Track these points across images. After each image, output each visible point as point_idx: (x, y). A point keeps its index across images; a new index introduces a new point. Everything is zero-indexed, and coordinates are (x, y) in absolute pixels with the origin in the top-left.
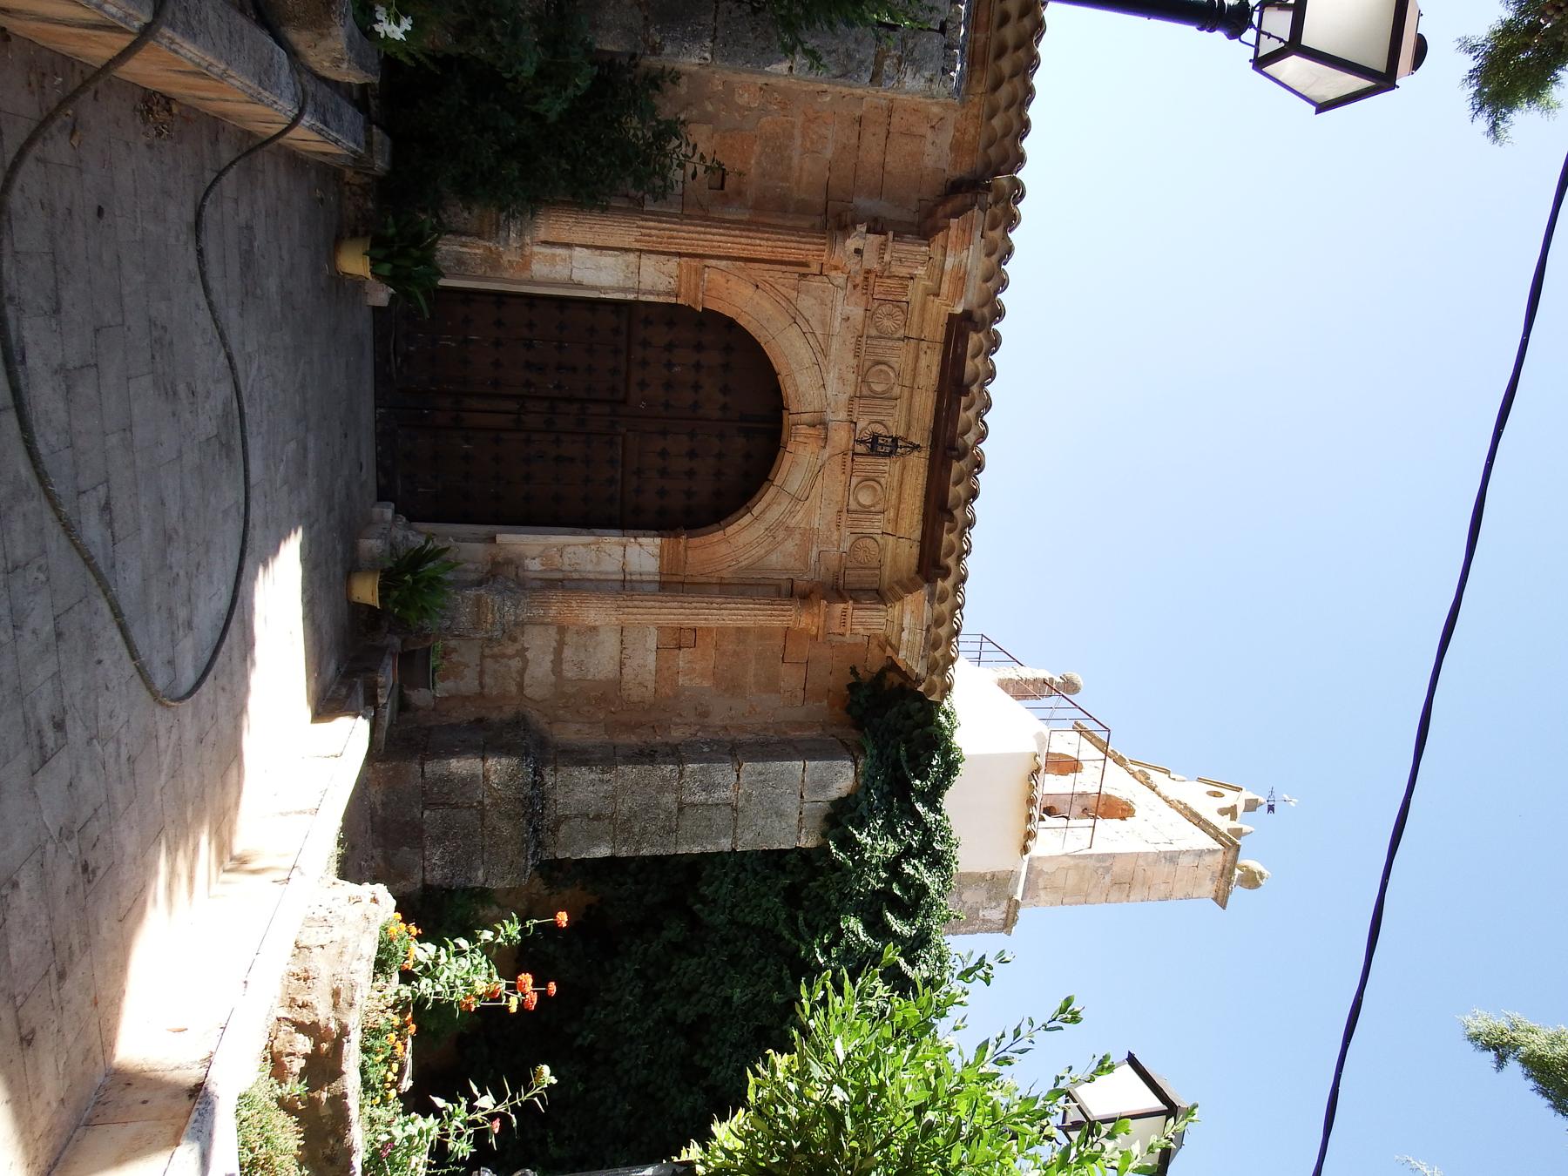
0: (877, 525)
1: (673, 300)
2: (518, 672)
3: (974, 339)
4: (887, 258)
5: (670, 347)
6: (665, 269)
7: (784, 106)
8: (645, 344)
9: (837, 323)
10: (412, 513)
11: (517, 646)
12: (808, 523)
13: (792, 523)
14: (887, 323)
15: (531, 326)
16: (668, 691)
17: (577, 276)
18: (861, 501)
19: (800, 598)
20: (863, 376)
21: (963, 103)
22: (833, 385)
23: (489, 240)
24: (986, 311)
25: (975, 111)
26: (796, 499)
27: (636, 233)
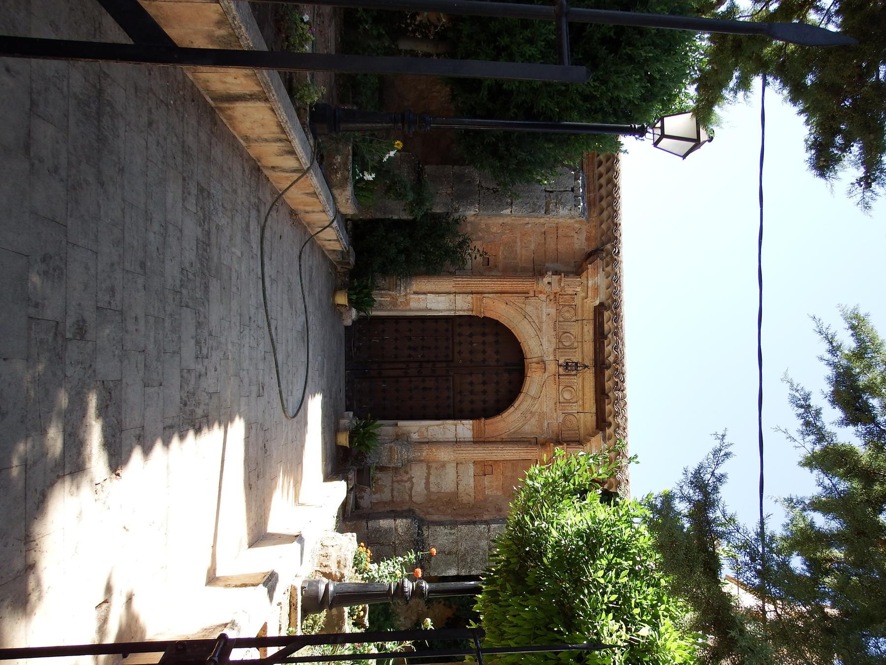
0: (575, 408)
1: (470, 313)
2: (409, 489)
3: (607, 314)
4: (562, 285)
5: (471, 335)
6: (466, 300)
7: (511, 230)
8: (460, 335)
9: (544, 317)
11: (408, 476)
12: (541, 409)
13: (534, 410)
14: (567, 315)
15: (410, 330)
16: (481, 497)
17: (429, 306)
18: (565, 397)
19: (541, 445)
21: (588, 220)
22: (546, 345)
23: (393, 291)
24: (610, 301)
25: (594, 224)
26: (534, 398)
27: (453, 284)
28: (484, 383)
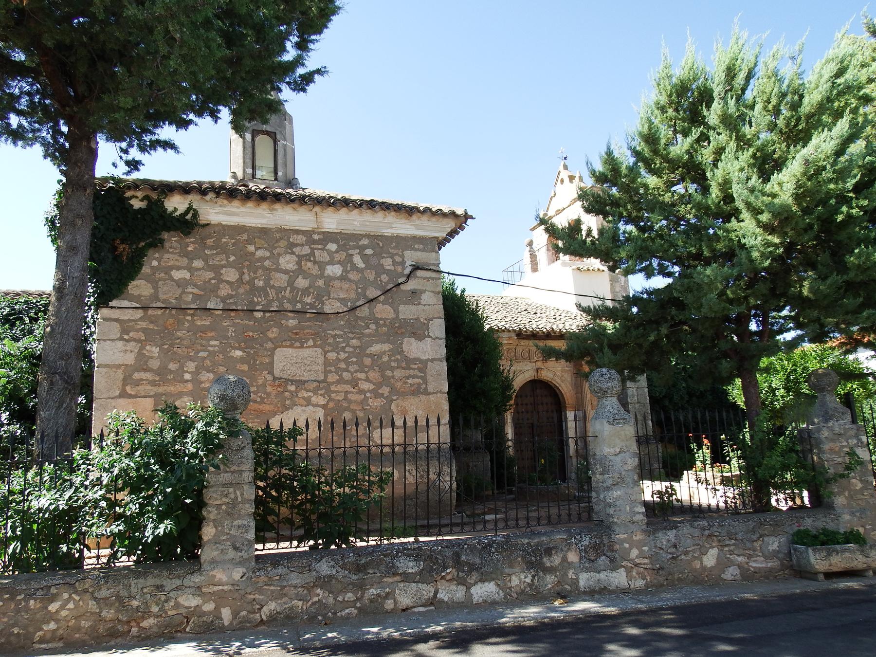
20: (525, 359)
22: (528, 368)
28: (542, 404)
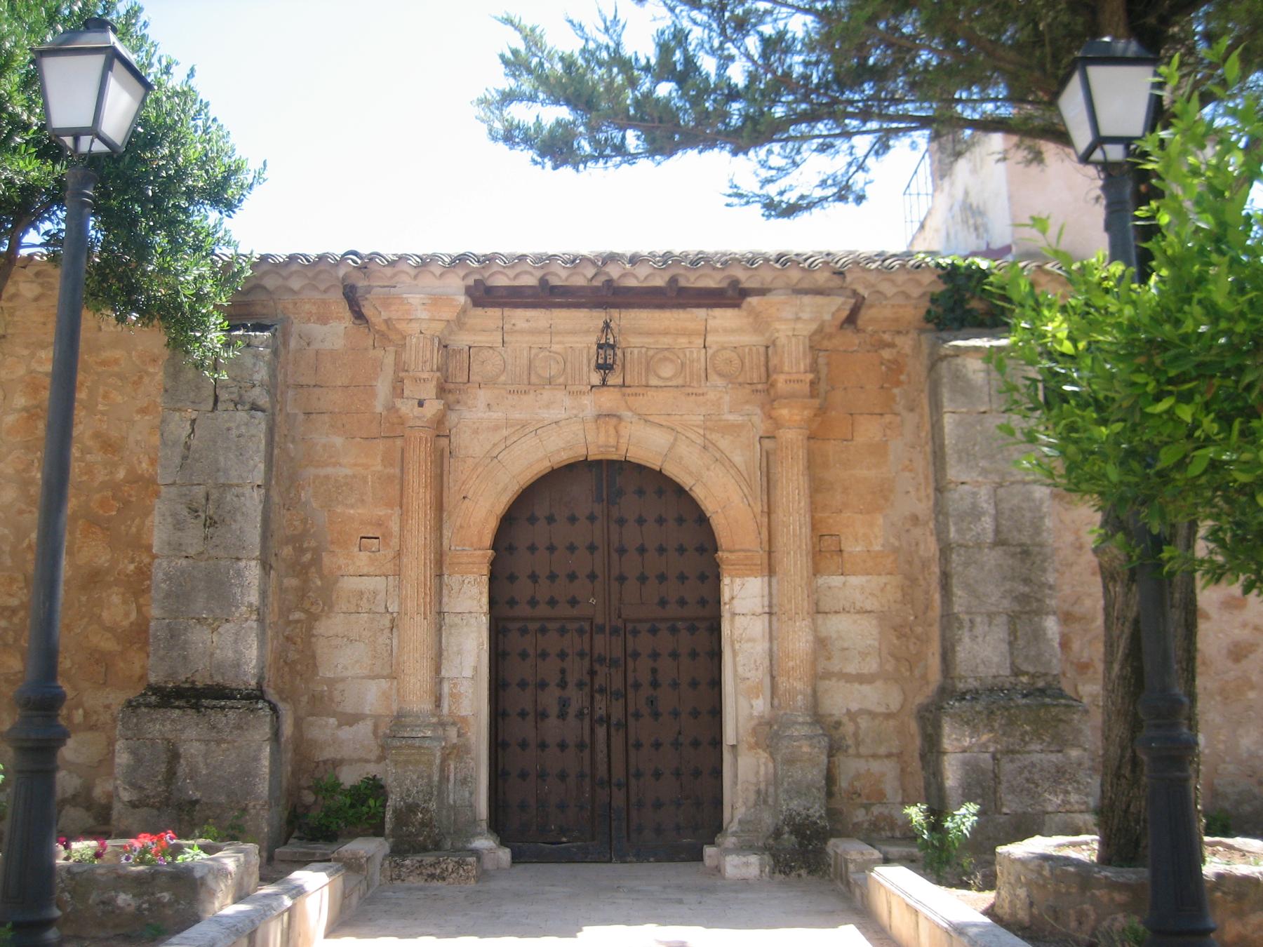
9: (495, 415)
10: (712, 827)
11: (845, 720)
